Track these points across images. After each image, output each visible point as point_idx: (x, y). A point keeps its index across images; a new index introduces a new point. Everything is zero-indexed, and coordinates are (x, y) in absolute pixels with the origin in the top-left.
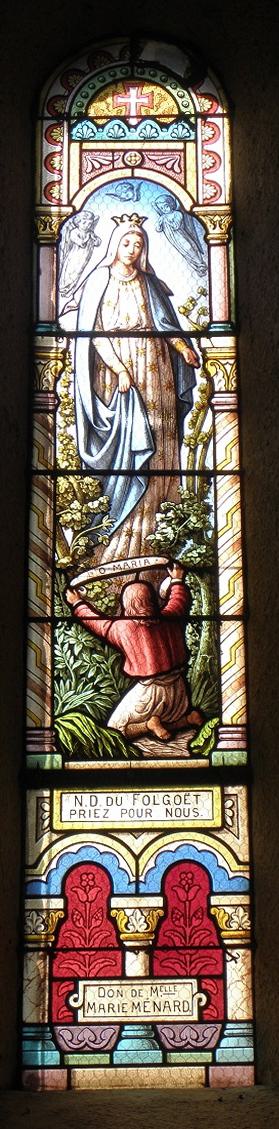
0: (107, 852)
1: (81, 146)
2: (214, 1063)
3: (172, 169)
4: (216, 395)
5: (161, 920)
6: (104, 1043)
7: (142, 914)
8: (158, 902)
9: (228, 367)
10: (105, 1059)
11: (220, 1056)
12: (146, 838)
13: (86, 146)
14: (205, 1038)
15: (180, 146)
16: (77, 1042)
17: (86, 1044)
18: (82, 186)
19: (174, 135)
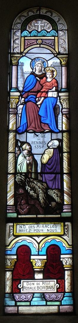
0: (51, 241)
1: (24, 38)
2: (61, 305)
3: (51, 44)
4: (63, 109)
5: (46, 263)
6: (59, 298)
7: (9, 261)
8: (45, 257)
10: (28, 303)
11: (32, 303)
12: (41, 238)
13: (26, 38)
14: (28, 298)
15: (53, 38)
16: (50, 298)
17: (54, 299)
18: (25, 49)
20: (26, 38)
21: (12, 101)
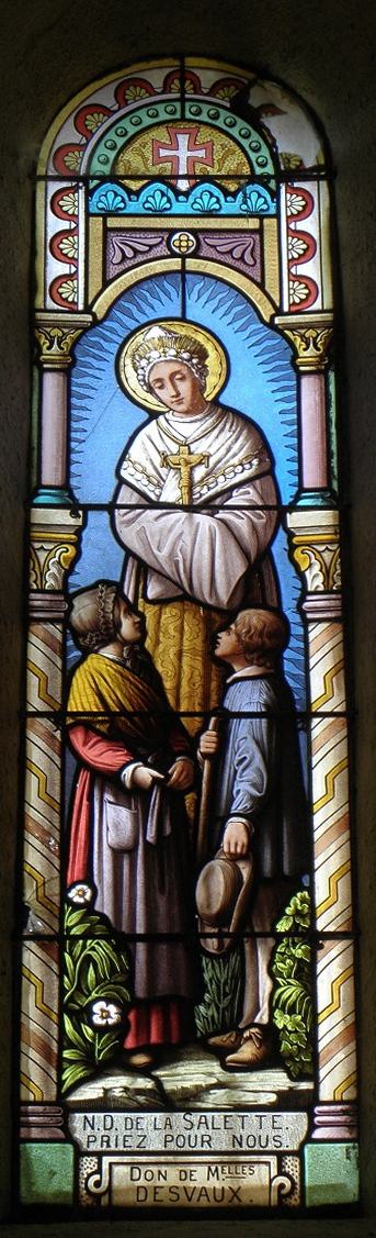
9: (327, 556)
19: (196, 206)
20: (112, 222)
21: (42, 556)
